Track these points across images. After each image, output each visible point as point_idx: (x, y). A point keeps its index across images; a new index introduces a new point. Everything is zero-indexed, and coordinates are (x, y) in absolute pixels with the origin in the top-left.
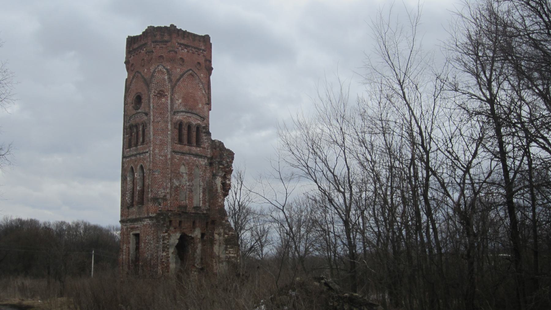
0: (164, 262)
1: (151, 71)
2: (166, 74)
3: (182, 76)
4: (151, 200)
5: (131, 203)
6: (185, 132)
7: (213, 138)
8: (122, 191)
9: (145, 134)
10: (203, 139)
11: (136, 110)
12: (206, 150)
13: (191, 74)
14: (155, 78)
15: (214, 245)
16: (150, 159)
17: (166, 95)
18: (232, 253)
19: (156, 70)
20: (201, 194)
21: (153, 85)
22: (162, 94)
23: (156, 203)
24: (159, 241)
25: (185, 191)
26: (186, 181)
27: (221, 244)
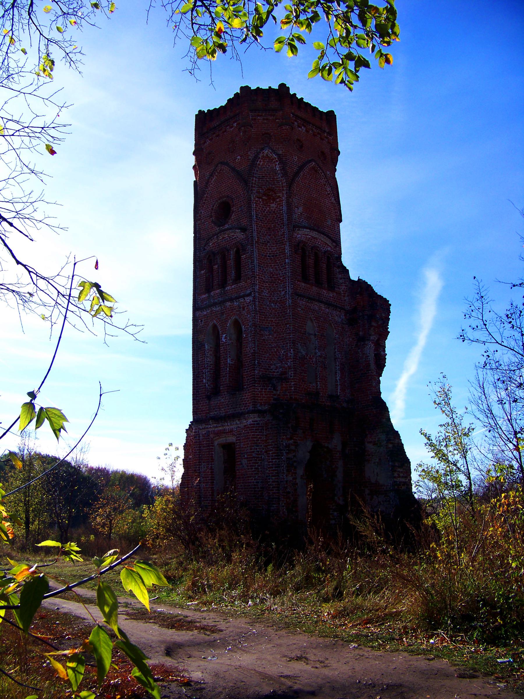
0: (289, 493)
1: (250, 158)
2: (277, 161)
3: (301, 168)
4: (259, 381)
6: (311, 261)
7: (354, 277)
10: (337, 278)
11: (219, 226)
12: (342, 297)
13: (313, 168)
17: (279, 197)
18: (403, 477)
25: (315, 366)
26: (316, 349)
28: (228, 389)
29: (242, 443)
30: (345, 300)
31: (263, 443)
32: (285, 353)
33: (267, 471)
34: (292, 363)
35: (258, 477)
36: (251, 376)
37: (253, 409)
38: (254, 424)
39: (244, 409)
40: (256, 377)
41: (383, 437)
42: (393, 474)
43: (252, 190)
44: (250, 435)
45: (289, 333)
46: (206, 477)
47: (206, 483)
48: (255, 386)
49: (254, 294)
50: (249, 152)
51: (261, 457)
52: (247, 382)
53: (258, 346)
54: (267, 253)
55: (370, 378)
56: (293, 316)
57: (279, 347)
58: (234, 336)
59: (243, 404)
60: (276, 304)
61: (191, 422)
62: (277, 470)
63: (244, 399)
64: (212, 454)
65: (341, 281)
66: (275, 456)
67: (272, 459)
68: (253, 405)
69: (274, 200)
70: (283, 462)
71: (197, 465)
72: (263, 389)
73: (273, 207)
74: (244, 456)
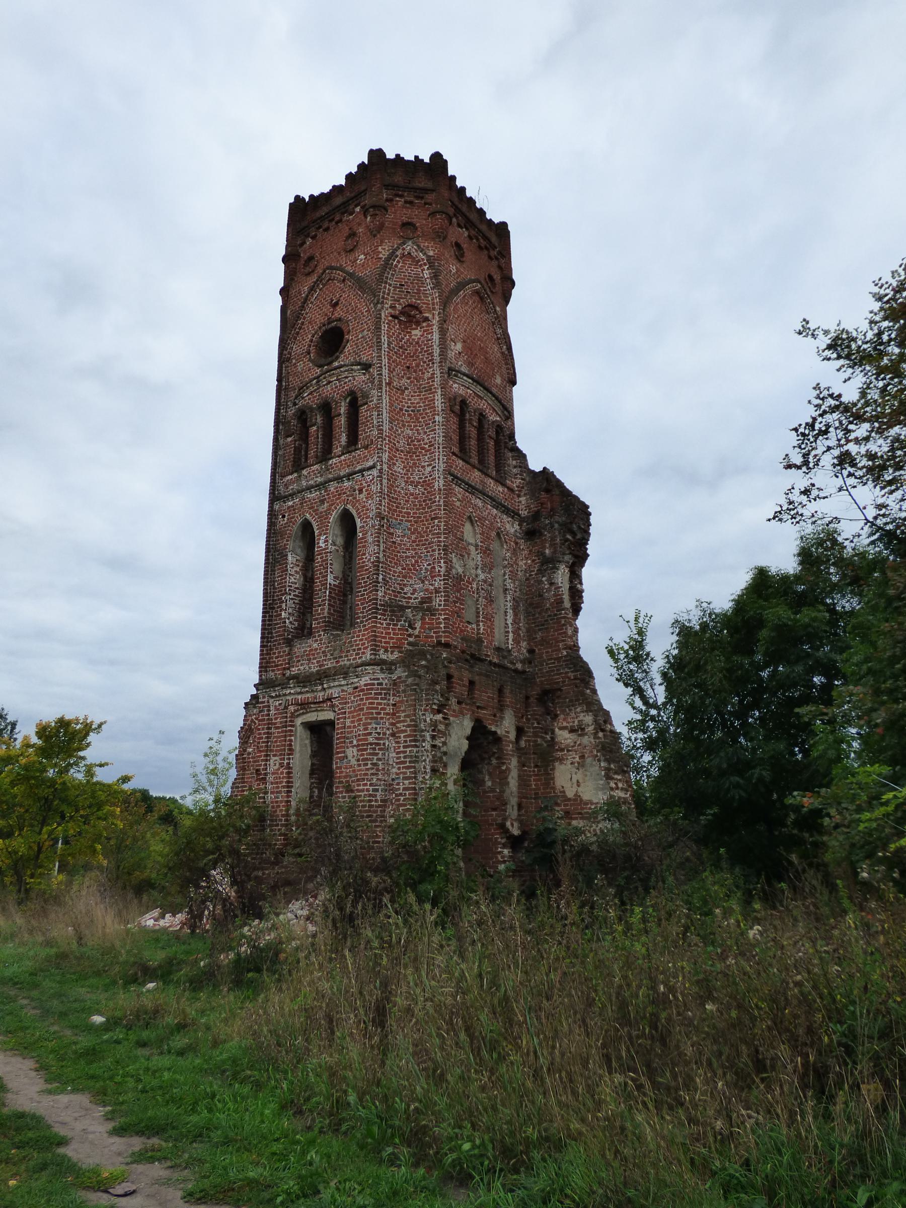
1: (381, 256)
2: (425, 264)
4: (385, 611)
5: (295, 628)
8: (266, 594)
9: (362, 419)
10: (509, 466)
14: (395, 271)
15: (557, 764)
16: (381, 484)
17: (426, 319)
19: (398, 253)
20: (510, 612)
21: (389, 290)
22: (414, 317)
23: (399, 621)
24: (418, 738)
25: (475, 595)
27: (589, 760)
28: (326, 626)
29: (349, 718)
30: (520, 502)
31: (389, 719)
32: (429, 567)
33: (394, 770)
34: (442, 583)
35: (378, 779)
36: (370, 601)
37: (373, 657)
38: (373, 684)
39: (354, 659)
40: (379, 602)
41: (588, 719)
42: (609, 783)
43: (383, 302)
44: (364, 704)
45: (438, 533)
46: (277, 783)
47: (277, 792)
48: (376, 618)
49: (381, 465)
50: (380, 248)
51: (384, 744)
52: (363, 613)
53: (384, 551)
54: (404, 406)
55: (563, 622)
56: (445, 505)
57: (420, 557)
58: (340, 541)
59: (354, 650)
60: (416, 486)
61: (463, 189)
62: (414, 767)
63: (356, 641)
64: (291, 741)
65: (515, 470)
66: (411, 741)
67: (404, 747)
68: (371, 650)
69: (418, 323)
70: (425, 753)
71: (262, 760)
72: (390, 624)
73: (416, 335)
74: (351, 742)
